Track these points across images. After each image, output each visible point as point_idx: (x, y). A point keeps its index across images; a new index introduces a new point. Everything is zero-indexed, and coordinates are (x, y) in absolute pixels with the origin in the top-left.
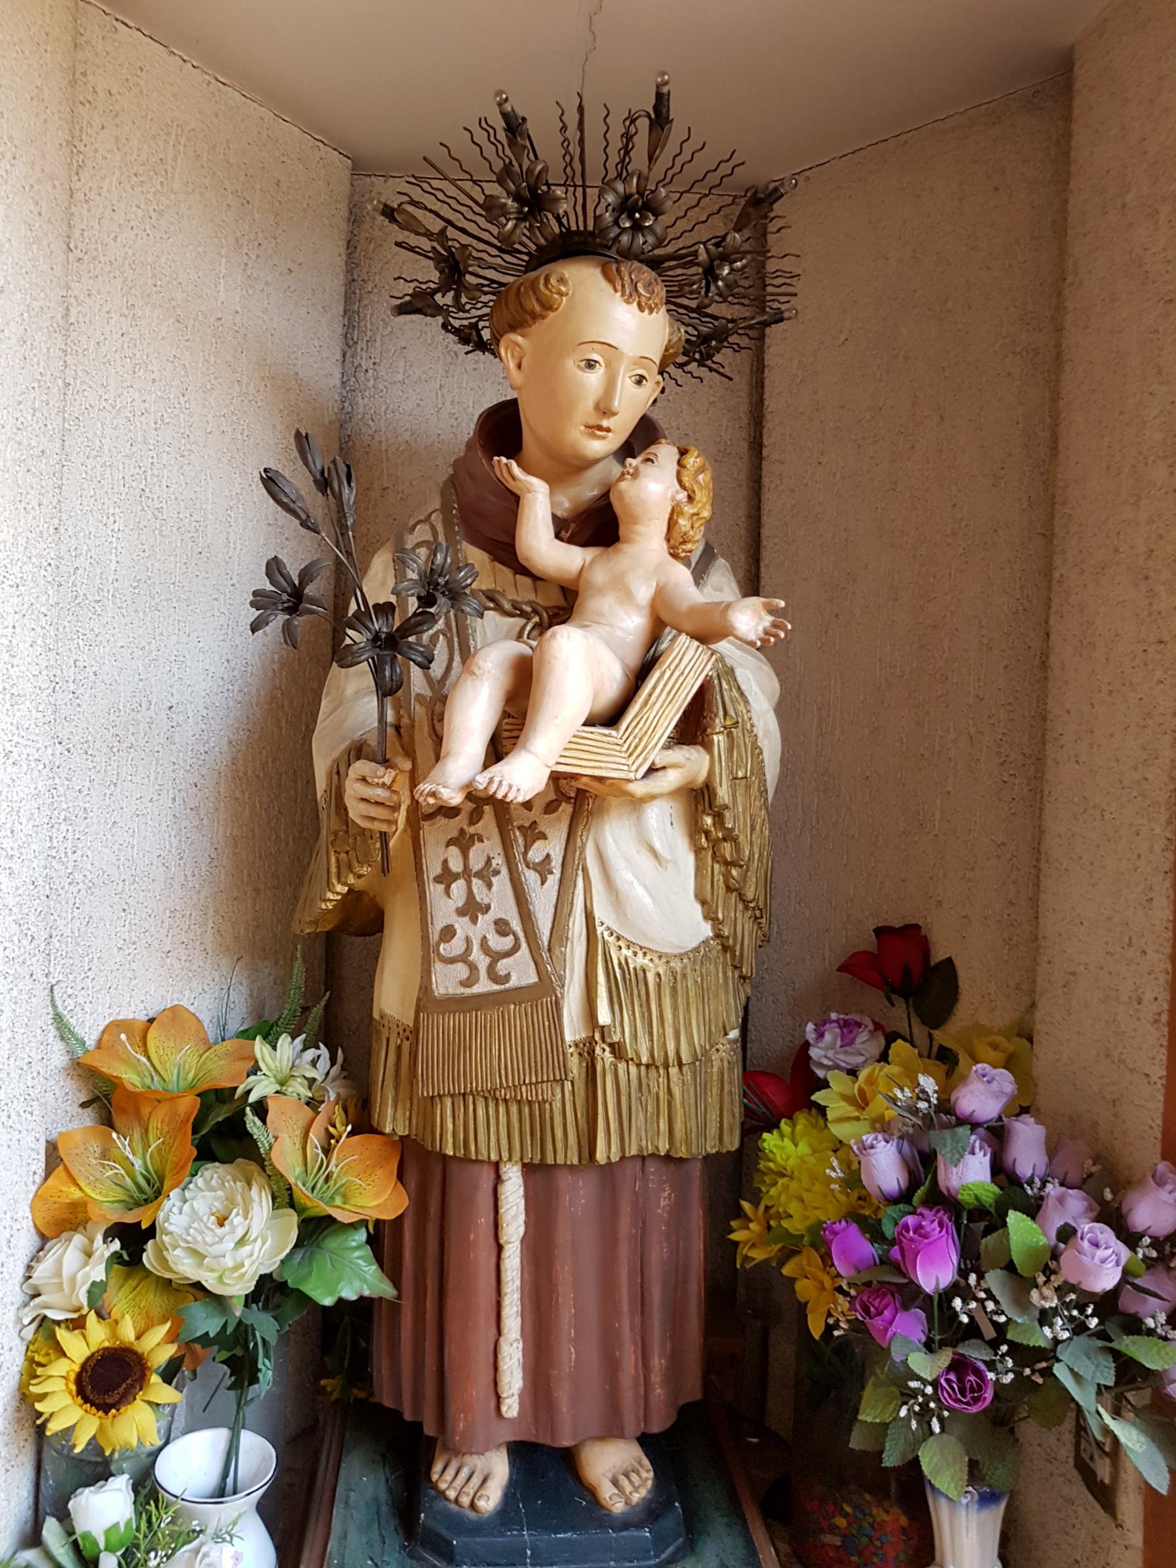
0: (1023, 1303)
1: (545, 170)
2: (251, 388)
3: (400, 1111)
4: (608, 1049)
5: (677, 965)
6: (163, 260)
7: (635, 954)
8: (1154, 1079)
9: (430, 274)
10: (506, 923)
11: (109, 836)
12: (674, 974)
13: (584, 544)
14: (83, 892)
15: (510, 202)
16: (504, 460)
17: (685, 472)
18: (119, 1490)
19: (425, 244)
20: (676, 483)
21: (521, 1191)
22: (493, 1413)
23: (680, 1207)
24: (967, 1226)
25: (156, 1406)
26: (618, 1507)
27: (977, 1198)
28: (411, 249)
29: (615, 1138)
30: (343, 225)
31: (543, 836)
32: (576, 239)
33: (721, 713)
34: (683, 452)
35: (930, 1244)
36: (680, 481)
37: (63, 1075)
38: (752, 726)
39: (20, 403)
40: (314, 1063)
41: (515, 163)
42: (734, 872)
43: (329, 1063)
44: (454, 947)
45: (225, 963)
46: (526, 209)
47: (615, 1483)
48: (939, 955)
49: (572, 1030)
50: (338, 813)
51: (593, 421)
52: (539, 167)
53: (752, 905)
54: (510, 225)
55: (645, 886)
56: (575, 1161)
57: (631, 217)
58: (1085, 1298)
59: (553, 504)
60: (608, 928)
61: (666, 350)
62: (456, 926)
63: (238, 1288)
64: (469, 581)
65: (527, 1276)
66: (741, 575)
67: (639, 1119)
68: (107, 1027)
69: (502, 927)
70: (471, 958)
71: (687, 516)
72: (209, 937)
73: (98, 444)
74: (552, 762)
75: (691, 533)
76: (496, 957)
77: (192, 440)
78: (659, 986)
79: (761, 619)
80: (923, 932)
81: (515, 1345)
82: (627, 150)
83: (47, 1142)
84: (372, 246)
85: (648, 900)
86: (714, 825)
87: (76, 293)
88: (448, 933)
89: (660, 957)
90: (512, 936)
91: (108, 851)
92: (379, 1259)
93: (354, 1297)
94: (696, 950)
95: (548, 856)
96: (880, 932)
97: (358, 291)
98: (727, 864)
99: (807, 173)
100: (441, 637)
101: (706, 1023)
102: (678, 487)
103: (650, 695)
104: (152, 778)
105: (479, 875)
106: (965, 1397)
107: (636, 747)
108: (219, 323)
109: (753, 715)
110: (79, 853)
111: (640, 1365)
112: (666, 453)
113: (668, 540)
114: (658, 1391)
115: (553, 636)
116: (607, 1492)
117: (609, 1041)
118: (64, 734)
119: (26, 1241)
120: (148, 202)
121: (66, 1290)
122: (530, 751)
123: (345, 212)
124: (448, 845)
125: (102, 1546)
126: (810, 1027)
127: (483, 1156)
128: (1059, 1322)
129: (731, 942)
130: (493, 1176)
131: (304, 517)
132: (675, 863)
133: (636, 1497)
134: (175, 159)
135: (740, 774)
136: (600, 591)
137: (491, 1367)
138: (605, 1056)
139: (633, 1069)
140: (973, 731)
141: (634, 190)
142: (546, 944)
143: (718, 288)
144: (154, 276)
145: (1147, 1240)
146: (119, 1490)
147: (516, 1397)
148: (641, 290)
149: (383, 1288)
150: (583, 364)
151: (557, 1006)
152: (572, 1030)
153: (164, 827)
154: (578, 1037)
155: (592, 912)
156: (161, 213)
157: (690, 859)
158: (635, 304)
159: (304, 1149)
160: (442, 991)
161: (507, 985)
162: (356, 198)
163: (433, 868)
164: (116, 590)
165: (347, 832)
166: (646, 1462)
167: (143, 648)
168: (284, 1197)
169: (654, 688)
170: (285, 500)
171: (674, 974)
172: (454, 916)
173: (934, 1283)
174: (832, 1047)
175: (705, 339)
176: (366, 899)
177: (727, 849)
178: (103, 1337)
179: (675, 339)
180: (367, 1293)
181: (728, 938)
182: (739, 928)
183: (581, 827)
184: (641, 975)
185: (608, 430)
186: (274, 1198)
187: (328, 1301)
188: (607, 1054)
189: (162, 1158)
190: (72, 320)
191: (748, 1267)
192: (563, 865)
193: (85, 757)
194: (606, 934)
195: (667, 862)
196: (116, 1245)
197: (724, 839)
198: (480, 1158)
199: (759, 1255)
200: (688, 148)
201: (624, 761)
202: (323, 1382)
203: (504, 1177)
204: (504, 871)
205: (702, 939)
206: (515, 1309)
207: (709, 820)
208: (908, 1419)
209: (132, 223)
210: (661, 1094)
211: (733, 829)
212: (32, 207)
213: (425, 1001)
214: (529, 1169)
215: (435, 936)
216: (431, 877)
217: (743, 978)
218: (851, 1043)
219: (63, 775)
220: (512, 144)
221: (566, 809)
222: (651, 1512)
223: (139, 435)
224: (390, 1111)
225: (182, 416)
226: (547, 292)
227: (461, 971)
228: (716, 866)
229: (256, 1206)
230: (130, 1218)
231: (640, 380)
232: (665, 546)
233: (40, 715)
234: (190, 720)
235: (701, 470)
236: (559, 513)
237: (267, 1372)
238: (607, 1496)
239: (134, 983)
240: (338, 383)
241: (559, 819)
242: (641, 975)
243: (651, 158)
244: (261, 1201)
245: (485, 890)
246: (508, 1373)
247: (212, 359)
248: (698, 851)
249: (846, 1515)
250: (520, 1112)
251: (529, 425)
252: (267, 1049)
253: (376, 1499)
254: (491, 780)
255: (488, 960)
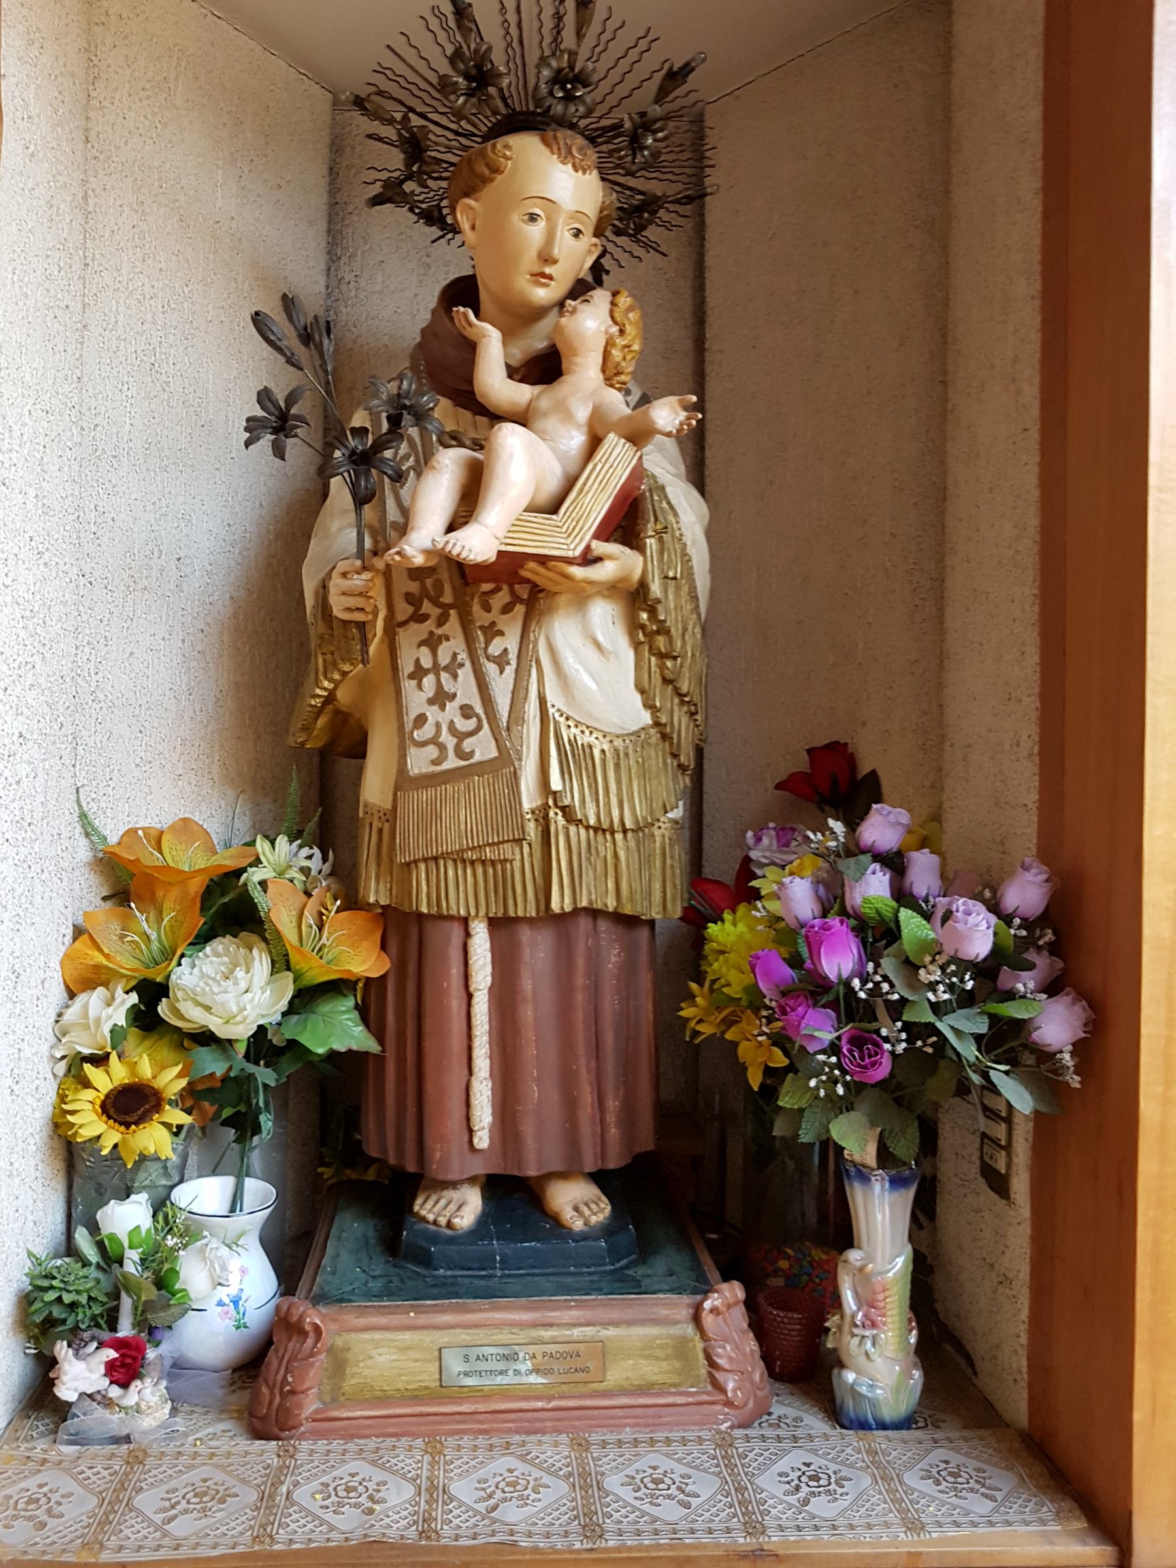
0: (913, 983)
1: (490, 49)
2: (246, 286)
3: (381, 884)
4: (560, 814)
5: (618, 743)
6: (168, 166)
7: (583, 732)
8: (1030, 805)
9: (395, 160)
10: (470, 707)
11: (126, 664)
12: (616, 751)
13: (533, 383)
14: (104, 710)
15: (461, 80)
16: (462, 309)
17: (616, 309)
18: (140, 1203)
19: (389, 132)
20: (609, 319)
21: (488, 945)
22: (466, 1146)
23: (628, 969)
24: (872, 943)
25: (167, 1125)
26: (578, 1225)
27: (878, 912)
28: (380, 140)
29: (567, 891)
30: (326, 151)
31: (501, 633)
32: (520, 117)
33: (652, 519)
34: (615, 294)
35: (832, 934)
36: (612, 317)
37: (86, 870)
38: (681, 535)
39: (48, 256)
40: (310, 857)
41: (464, 45)
42: (669, 664)
43: (321, 862)
44: (427, 731)
45: (230, 793)
46: (474, 85)
47: (576, 1209)
48: (864, 769)
49: (529, 799)
50: (323, 619)
51: (536, 270)
52: (484, 48)
53: (687, 699)
54: (461, 100)
55: (590, 674)
56: (534, 914)
57: (563, 88)
58: (965, 965)
59: (506, 355)
60: (559, 710)
61: (601, 212)
62: (428, 714)
63: (241, 1031)
64: (431, 405)
65: (494, 1024)
66: (688, 461)
67: (588, 877)
68: (126, 832)
69: (467, 711)
70: (441, 740)
71: (619, 347)
72: (215, 768)
73: (113, 320)
74: (501, 534)
75: (623, 364)
76: (461, 736)
77: (195, 325)
78: (604, 761)
79: (677, 414)
80: (850, 750)
81: (485, 1083)
82: (558, 29)
83: (74, 925)
84: (353, 172)
85: (592, 685)
86: (649, 619)
87: (94, 186)
88: (421, 720)
89: (604, 736)
90: (475, 719)
91: (126, 677)
92: (365, 1020)
93: (343, 1050)
94: (636, 734)
95: (506, 650)
96: (811, 751)
97: (341, 213)
98: (662, 656)
99: (737, 93)
100: (412, 473)
101: (648, 799)
102: (611, 322)
103: (585, 484)
104: (164, 619)
105: (446, 669)
106: (863, 1060)
107: (574, 529)
108: (216, 226)
109: (681, 525)
110: (100, 674)
111: (596, 1106)
112: (600, 297)
113: (603, 371)
114: (613, 1131)
115: (500, 429)
116: (568, 1215)
117: (560, 804)
118: (87, 569)
119: (57, 992)
120: (154, 114)
121: (92, 1028)
122: (481, 523)
123: (327, 140)
124: (420, 645)
125: (126, 1245)
126: (750, 834)
127: (454, 912)
128: (941, 988)
129: (668, 729)
130: (462, 933)
131: (289, 354)
132: (617, 656)
133: (594, 1219)
134: (177, 79)
135: (671, 574)
136: (546, 414)
137: (463, 1103)
138: (557, 819)
139: (582, 831)
140: (888, 564)
141: (565, 65)
142: (505, 720)
143: (643, 156)
144: (160, 179)
145: (1017, 921)
146: (140, 1203)
147: (487, 1131)
148: (575, 152)
149: (370, 1044)
150: (526, 217)
151: (515, 776)
152: (529, 799)
153: (175, 664)
154: (534, 805)
155: (544, 697)
156: (165, 125)
157: (630, 655)
158: (570, 165)
159: (300, 927)
160: (416, 771)
161: (472, 761)
162: (338, 130)
163: (407, 667)
164: (131, 449)
165: (331, 635)
166: (604, 1198)
167: (154, 503)
168: (281, 963)
169: (588, 478)
170: (272, 338)
171: (616, 751)
172: (426, 706)
173: (836, 970)
174: (768, 849)
175: (638, 209)
176: (352, 720)
177: (661, 641)
178: (124, 1074)
179: (608, 202)
180: (355, 1048)
181: (665, 725)
182: (676, 719)
183: (534, 624)
184: (587, 751)
185: (550, 278)
186: (273, 962)
187: (321, 1051)
188: (560, 817)
189: (173, 933)
190: (90, 209)
191: (697, 1042)
192: (519, 657)
193: (105, 591)
194: (557, 715)
195: (610, 653)
196: (134, 998)
197: (658, 632)
198: (451, 913)
199: (706, 1029)
200: (612, 25)
201: (563, 541)
202: (320, 1170)
203: (472, 933)
204: (468, 664)
205: (642, 725)
206: (484, 1051)
207: (644, 616)
208: (817, 1088)
209: (141, 131)
210: (609, 857)
211: (664, 621)
212: (57, 94)
213: (403, 782)
214: (494, 924)
215: (409, 724)
216: (406, 674)
217: (680, 766)
218: (787, 845)
219: (87, 604)
220: (460, 26)
221: (520, 609)
222: (609, 1231)
223: (149, 315)
224: (373, 883)
225: (186, 304)
226: (494, 157)
227: (432, 751)
228: (653, 659)
229: (257, 963)
230: (149, 974)
231: (577, 233)
232: (601, 377)
233: (66, 533)
234: (197, 573)
235: (630, 309)
236: (513, 363)
237: (267, 1122)
238: (568, 1217)
239: (149, 797)
240: (323, 289)
241: (514, 618)
242: (587, 751)
243: (580, 35)
244: (261, 963)
245: (451, 680)
246: (479, 1108)
247: (211, 257)
248: (636, 645)
249: (789, 1258)
250: (485, 873)
251: (485, 285)
252: (267, 845)
253: (365, 1236)
254: (447, 542)
255: (455, 740)
